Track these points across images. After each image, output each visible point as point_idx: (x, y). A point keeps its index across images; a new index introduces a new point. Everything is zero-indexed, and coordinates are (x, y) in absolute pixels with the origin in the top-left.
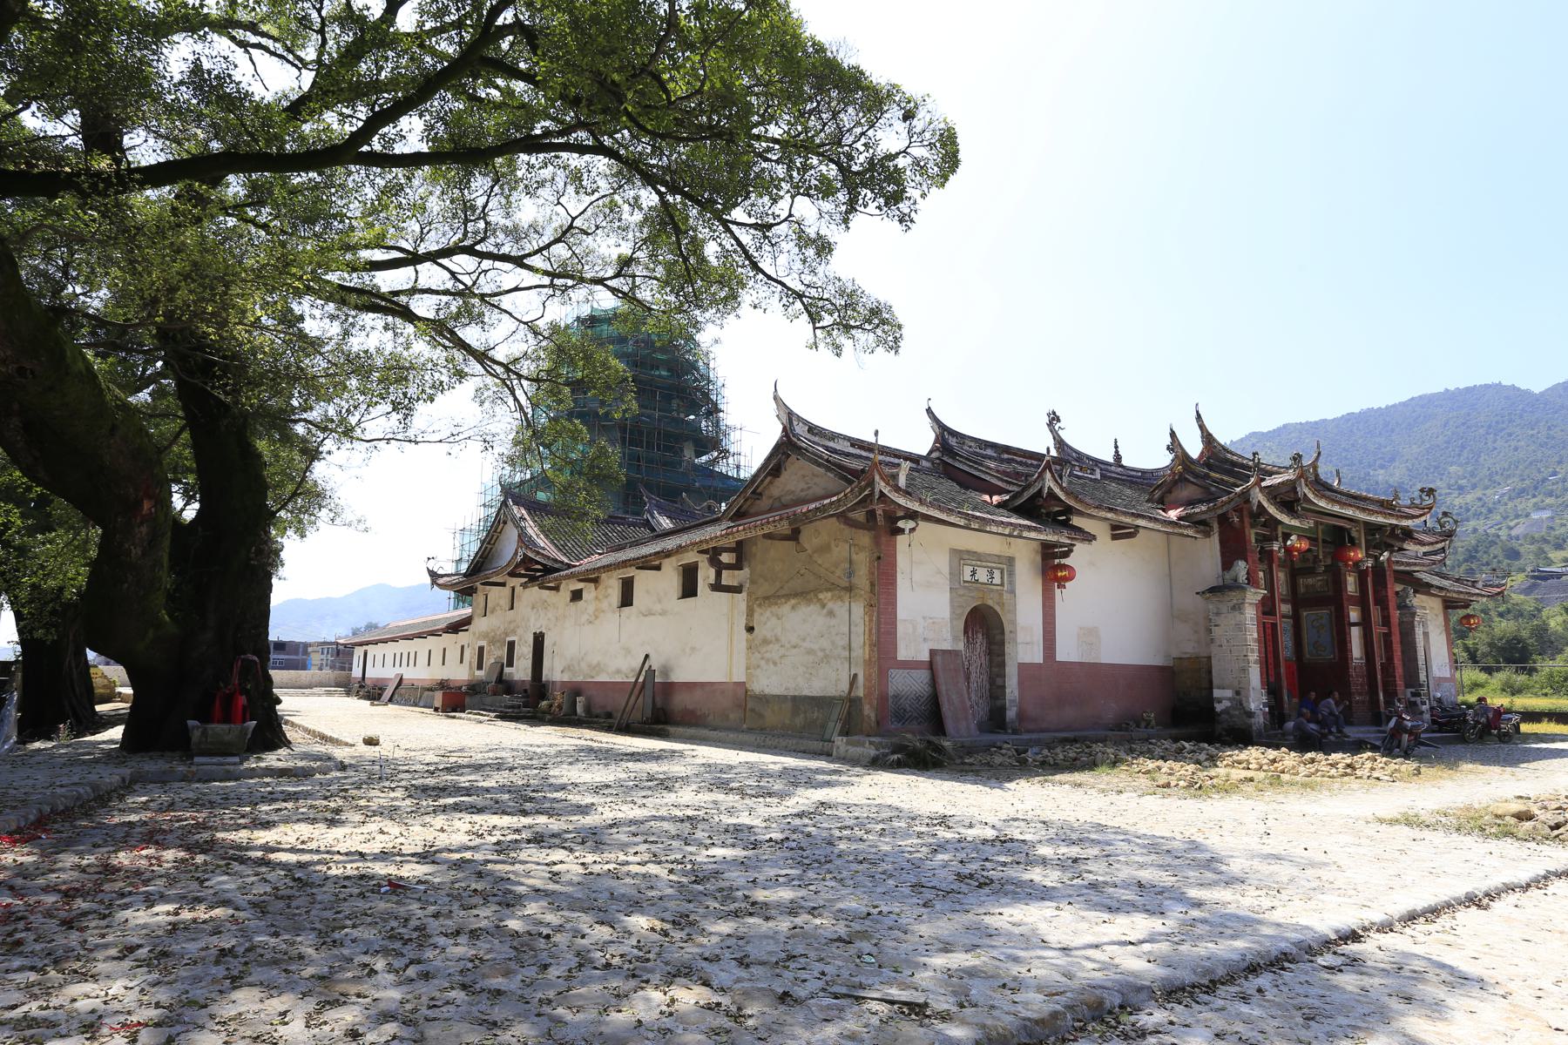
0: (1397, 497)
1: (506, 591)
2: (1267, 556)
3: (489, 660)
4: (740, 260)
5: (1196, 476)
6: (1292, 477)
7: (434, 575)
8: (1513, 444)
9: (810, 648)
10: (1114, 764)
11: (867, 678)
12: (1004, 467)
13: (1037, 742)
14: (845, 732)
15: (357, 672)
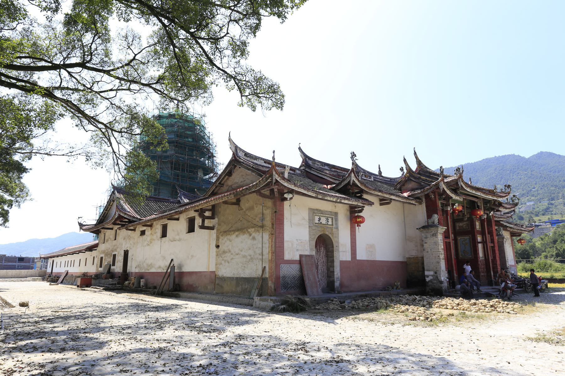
0: (495, 188)
1: (113, 232)
2: (445, 212)
3: (105, 263)
4: (204, 59)
5: (415, 178)
6: (456, 178)
7: (81, 225)
8: (519, 177)
9: (244, 256)
10: (386, 308)
11: (270, 268)
12: (332, 173)
13: (349, 297)
14: (260, 295)
15: (49, 270)
